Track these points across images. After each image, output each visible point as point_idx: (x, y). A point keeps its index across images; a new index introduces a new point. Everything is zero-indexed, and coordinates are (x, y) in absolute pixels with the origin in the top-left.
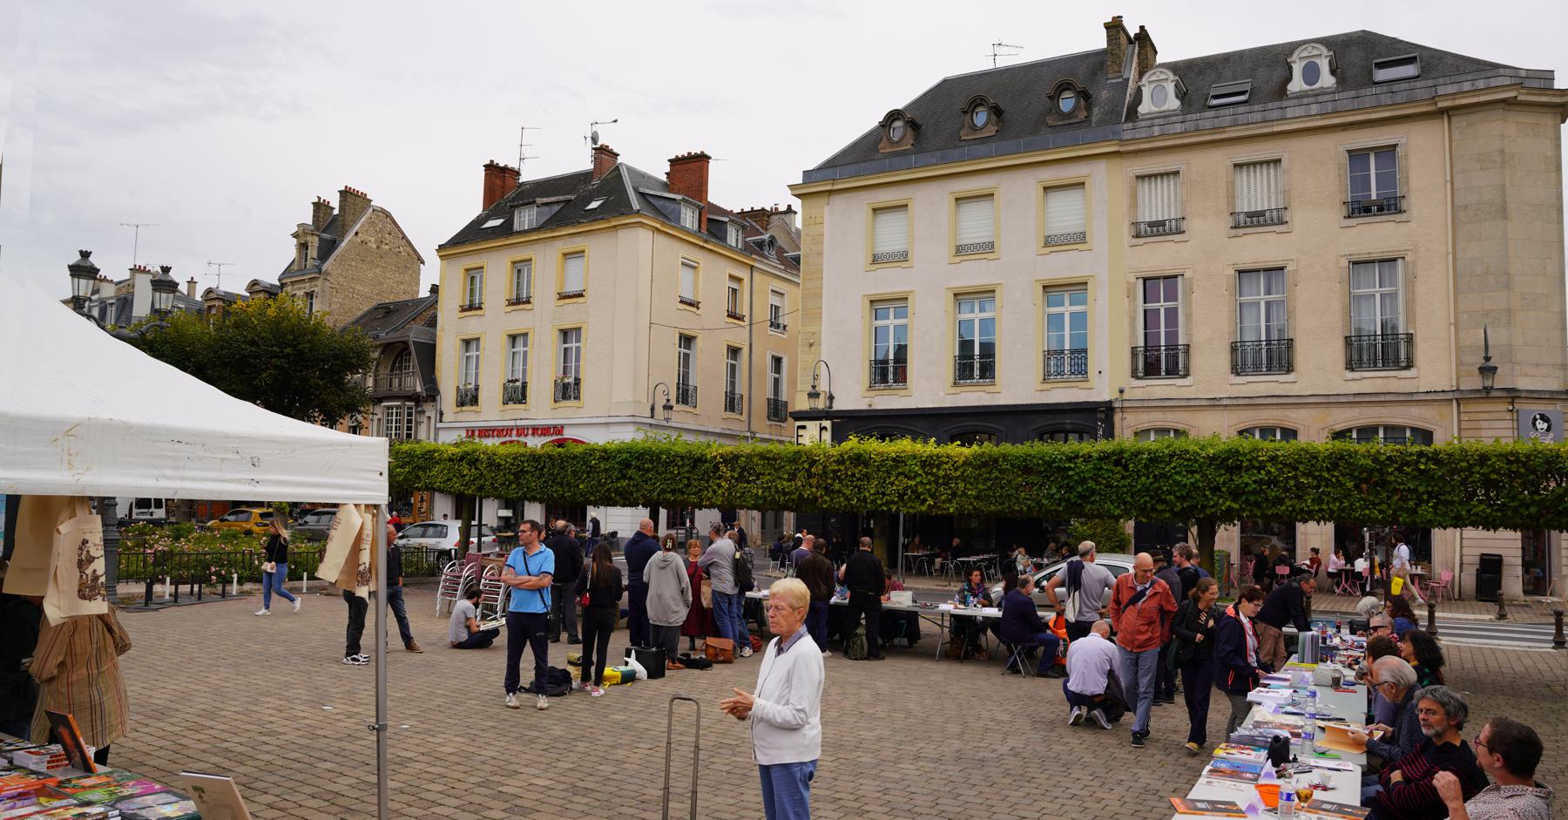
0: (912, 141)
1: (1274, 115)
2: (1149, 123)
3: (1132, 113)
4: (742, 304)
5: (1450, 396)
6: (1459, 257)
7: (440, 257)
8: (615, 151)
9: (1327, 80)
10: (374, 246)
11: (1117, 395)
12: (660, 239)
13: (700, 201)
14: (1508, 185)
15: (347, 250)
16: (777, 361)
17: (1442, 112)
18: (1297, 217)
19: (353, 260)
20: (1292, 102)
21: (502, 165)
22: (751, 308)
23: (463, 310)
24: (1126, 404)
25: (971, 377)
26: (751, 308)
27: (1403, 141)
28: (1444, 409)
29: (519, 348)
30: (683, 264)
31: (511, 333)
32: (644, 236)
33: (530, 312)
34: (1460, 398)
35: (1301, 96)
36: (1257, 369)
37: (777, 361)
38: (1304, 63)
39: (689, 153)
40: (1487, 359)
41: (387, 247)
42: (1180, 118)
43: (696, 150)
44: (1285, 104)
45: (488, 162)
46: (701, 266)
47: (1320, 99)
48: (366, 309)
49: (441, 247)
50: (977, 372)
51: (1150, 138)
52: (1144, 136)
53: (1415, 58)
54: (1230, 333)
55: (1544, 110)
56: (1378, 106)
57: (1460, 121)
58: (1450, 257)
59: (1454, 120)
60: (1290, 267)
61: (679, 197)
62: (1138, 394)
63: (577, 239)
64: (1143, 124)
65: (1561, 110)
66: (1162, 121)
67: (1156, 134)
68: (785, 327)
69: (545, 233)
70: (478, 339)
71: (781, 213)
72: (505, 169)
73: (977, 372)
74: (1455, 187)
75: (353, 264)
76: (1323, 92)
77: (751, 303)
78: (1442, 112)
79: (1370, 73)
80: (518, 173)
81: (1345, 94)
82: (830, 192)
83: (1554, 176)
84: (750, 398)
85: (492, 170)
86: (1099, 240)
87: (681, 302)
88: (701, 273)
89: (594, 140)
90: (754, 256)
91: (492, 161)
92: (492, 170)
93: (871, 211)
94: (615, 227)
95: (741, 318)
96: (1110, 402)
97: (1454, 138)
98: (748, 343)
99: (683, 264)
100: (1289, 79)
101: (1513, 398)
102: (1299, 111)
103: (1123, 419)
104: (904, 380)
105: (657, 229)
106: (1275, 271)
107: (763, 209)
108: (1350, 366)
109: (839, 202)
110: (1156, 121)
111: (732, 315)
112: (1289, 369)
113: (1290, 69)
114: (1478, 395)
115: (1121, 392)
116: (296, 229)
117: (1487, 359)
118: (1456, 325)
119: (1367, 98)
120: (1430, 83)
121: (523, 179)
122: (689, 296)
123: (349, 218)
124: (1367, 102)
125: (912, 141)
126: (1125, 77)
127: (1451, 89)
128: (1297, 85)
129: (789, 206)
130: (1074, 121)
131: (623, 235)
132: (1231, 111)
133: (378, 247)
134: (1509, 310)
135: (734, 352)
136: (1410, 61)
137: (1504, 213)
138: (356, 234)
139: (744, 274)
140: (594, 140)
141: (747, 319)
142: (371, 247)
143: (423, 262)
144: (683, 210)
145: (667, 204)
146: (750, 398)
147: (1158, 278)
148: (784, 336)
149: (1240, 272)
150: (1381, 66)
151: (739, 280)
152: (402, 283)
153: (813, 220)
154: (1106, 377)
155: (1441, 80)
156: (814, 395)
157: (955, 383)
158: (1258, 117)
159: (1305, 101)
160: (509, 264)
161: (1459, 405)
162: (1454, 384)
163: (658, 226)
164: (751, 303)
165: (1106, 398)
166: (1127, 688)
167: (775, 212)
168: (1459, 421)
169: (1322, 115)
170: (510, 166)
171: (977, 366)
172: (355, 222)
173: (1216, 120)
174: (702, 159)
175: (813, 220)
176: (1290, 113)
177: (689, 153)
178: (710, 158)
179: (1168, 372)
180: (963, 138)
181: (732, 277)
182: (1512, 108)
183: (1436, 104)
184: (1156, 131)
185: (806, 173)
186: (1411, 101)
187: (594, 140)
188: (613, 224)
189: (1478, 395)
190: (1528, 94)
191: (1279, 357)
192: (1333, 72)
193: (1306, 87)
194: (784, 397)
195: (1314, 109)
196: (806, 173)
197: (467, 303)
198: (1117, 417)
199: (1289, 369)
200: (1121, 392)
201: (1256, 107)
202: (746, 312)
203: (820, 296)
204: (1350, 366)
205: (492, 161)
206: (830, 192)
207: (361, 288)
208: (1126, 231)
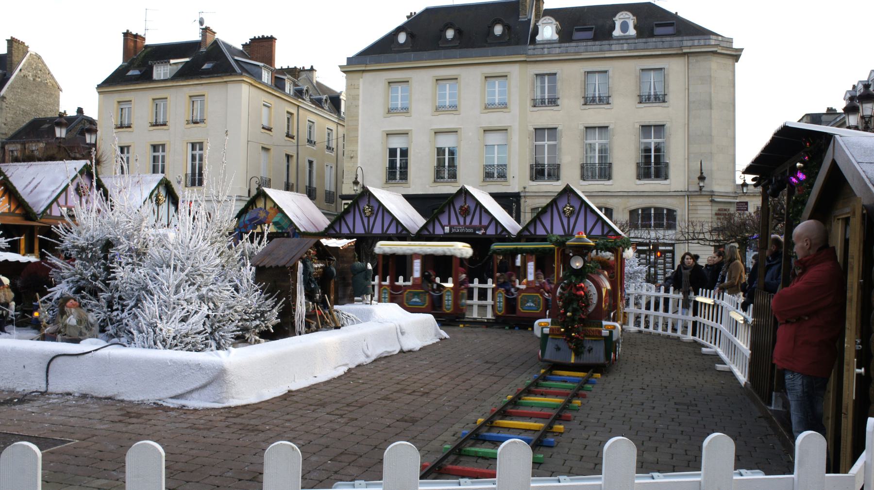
0: (411, 45)
1: (606, 47)
2: (542, 46)
3: (533, 41)
4: (293, 129)
5: (684, 194)
6: (690, 126)
7: (98, 92)
8: (214, 30)
9: (632, 32)
10: (32, 79)
11: (523, 189)
12: (253, 89)
13: (271, 66)
14: (712, 92)
15: (15, 81)
16: (311, 163)
17: (684, 54)
18: (614, 100)
19: (19, 88)
20: (615, 42)
21: (134, 33)
22: (298, 131)
23: (117, 128)
24: (527, 194)
25: (395, 179)
26: (298, 131)
27: (666, 67)
28: (682, 200)
29: (197, 152)
30: (264, 105)
31: (288, 153)
32: (245, 88)
33: (166, 131)
34: (689, 195)
35: (619, 39)
36: (593, 178)
37: (311, 163)
38: (622, 21)
39: (263, 36)
40: (702, 173)
41: (39, 80)
42: (558, 45)
43: (267, 34)
44: (611, 42)
45: (125, 31)
46: (273, 106)
47: (629, 41)
48: (27, 122)
49: (99, 86)
50: (398, 176)
51: (543, 55)
52: (539, 53)
53: (673, 23)
54: (580, 159)
55: (729, 57)
56: (656, 48)
57: (693, 59)
58: (687, 126)
59: (690, 58)
60: (611, 127)
61: (261, 64)
62: (534, 189)
63: (199, 87)
64: (539, 46)
65: (735, 58)
66: (549, 46)
67: (546, 53)
68: (315, 142)
69: (177, 82)
70: (163, 145)
71: (307, 70)
72: (136, 36)
73: (398, 176)
74: (690, 92)
75: (19, 91)
76: (629, 38)
77: (298, 129)
78: (684, 54)
79: (652, 30)
80: (144, 39)
81: (641, 40)
82: (363, 71)
83: (732, 89)
84: (297, 185)
85: (127, 35)
86: (515, 107)
87: (263, 128)
88: (273, 110)
89: (201, 23)
90: (300, 100)
91: (128, 31)
92: (127, 35)
93: (387, 84)
94: (226, 82)
95: (292, 138)
96: (519, 193)
97: (690, 67)
98: (296, 153)
99: (264, 105)
100: (614, 28)
101: (712, 195)
102: (617, 47)
103: (525, 202)
104: (406, 179)
105: (251, 84)
106: (604, 128)
107: (295, 68)
108: (639, 177)
109: (367, 76)
110: (546, 46)
111: (288, 135)
112: (609, 177)
113: (614, 24)
114: (696, 194)
115: (525, 188)
116: (10, 38)
117: (702, 173)
118: (688, 159)
119: (651, 43)
120: (680, 38)
121: (148, 42)
122: (266, 124)
123: (15, 59)
124: (651, 45)
125: (411, 45)
126: (529, 18)
127: (689, 43)
128: (617, 32)
129: (312, 67)
130: (501, 41)
131: (231, 86)
132: (584, 44)
133: (34, 80)
134: (711, 153)
135: (288, 157)
136: (671, 25)
137: (710, 107)
138: (21, 70)
139: (293, 110)
140: (201, 22)
141: (295, 138)
142: (30, 80)
143: (61, 91)
144: (263, 71)
145: (253, 67)
146: (297, 185)
147: (544, 129)
148: (314, 148)
149: (587, 128)
150: (658, 25)
151: (292, 114)
152: (49, 104)
153: (353, 87)
154: (516, 179)
155: (685, 38)
156: (356, 183)
157: (435, 181)
158: (598, 48)
159: (621, 42)
160: (151, 100)
161: (688, 198)
162: (686, 188)
163: (252, 82)
164: (298, 129)
165: (516, 190)
166: (521, 402)
167: (303, 70)
168: (688, 206)
169: (630, 50)
170: (139, 34)
171: (398, 173)
172: (19, 63)
173: (577, 48)
174: (270, 41)
175: (353, 87)
176: (613, 47)
177: (263, 36)
178: (276, 39)
179: (401, 179)
180: (440, 45)
181: (288, 112)
182: (715, 55)
183: (682, 50)
184: (546, 51)
185: (349, 59)
186: (671, 47)
187: (201, 23)
188: (225, 80)
189: (696, 194)
190: (722, 49)
191: (605, 172)
192: (635, 27)
193: (622, 34)
194: (314, 185)
195: (625, 46)
196: (349, 59)
197: (119, 123)
198: (522, 200)
199: (609, 177)
200: (525, 188)
201: (597, 43)
202: (295, 134)
203: (357, 130)
204: (639, 177)
205: (128, 31)
206: (363, 71)
207: (24, 107)
208: (529, 103)
